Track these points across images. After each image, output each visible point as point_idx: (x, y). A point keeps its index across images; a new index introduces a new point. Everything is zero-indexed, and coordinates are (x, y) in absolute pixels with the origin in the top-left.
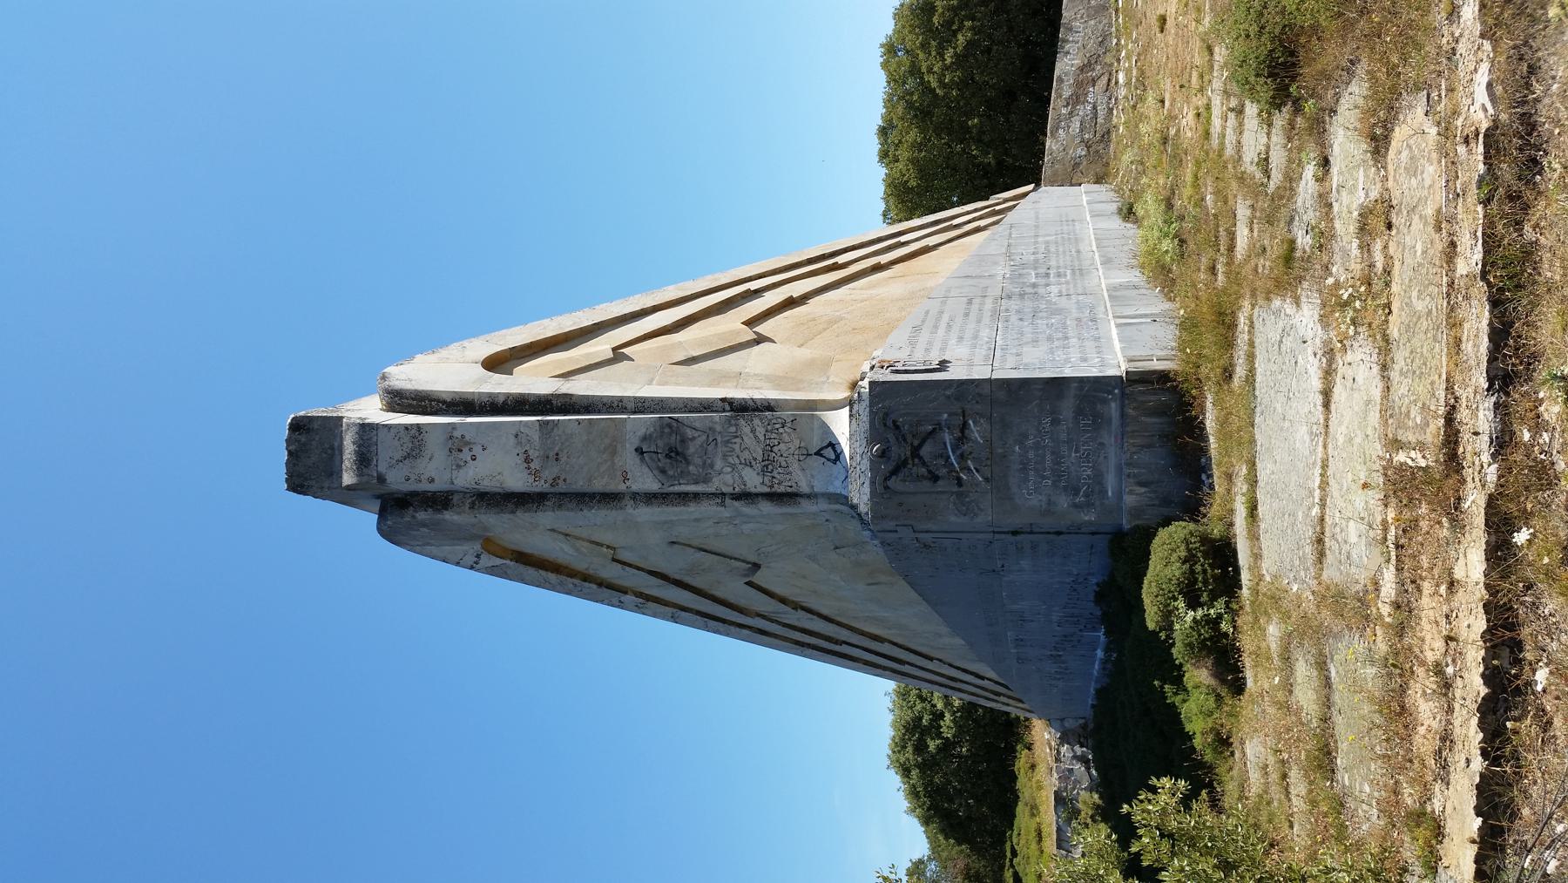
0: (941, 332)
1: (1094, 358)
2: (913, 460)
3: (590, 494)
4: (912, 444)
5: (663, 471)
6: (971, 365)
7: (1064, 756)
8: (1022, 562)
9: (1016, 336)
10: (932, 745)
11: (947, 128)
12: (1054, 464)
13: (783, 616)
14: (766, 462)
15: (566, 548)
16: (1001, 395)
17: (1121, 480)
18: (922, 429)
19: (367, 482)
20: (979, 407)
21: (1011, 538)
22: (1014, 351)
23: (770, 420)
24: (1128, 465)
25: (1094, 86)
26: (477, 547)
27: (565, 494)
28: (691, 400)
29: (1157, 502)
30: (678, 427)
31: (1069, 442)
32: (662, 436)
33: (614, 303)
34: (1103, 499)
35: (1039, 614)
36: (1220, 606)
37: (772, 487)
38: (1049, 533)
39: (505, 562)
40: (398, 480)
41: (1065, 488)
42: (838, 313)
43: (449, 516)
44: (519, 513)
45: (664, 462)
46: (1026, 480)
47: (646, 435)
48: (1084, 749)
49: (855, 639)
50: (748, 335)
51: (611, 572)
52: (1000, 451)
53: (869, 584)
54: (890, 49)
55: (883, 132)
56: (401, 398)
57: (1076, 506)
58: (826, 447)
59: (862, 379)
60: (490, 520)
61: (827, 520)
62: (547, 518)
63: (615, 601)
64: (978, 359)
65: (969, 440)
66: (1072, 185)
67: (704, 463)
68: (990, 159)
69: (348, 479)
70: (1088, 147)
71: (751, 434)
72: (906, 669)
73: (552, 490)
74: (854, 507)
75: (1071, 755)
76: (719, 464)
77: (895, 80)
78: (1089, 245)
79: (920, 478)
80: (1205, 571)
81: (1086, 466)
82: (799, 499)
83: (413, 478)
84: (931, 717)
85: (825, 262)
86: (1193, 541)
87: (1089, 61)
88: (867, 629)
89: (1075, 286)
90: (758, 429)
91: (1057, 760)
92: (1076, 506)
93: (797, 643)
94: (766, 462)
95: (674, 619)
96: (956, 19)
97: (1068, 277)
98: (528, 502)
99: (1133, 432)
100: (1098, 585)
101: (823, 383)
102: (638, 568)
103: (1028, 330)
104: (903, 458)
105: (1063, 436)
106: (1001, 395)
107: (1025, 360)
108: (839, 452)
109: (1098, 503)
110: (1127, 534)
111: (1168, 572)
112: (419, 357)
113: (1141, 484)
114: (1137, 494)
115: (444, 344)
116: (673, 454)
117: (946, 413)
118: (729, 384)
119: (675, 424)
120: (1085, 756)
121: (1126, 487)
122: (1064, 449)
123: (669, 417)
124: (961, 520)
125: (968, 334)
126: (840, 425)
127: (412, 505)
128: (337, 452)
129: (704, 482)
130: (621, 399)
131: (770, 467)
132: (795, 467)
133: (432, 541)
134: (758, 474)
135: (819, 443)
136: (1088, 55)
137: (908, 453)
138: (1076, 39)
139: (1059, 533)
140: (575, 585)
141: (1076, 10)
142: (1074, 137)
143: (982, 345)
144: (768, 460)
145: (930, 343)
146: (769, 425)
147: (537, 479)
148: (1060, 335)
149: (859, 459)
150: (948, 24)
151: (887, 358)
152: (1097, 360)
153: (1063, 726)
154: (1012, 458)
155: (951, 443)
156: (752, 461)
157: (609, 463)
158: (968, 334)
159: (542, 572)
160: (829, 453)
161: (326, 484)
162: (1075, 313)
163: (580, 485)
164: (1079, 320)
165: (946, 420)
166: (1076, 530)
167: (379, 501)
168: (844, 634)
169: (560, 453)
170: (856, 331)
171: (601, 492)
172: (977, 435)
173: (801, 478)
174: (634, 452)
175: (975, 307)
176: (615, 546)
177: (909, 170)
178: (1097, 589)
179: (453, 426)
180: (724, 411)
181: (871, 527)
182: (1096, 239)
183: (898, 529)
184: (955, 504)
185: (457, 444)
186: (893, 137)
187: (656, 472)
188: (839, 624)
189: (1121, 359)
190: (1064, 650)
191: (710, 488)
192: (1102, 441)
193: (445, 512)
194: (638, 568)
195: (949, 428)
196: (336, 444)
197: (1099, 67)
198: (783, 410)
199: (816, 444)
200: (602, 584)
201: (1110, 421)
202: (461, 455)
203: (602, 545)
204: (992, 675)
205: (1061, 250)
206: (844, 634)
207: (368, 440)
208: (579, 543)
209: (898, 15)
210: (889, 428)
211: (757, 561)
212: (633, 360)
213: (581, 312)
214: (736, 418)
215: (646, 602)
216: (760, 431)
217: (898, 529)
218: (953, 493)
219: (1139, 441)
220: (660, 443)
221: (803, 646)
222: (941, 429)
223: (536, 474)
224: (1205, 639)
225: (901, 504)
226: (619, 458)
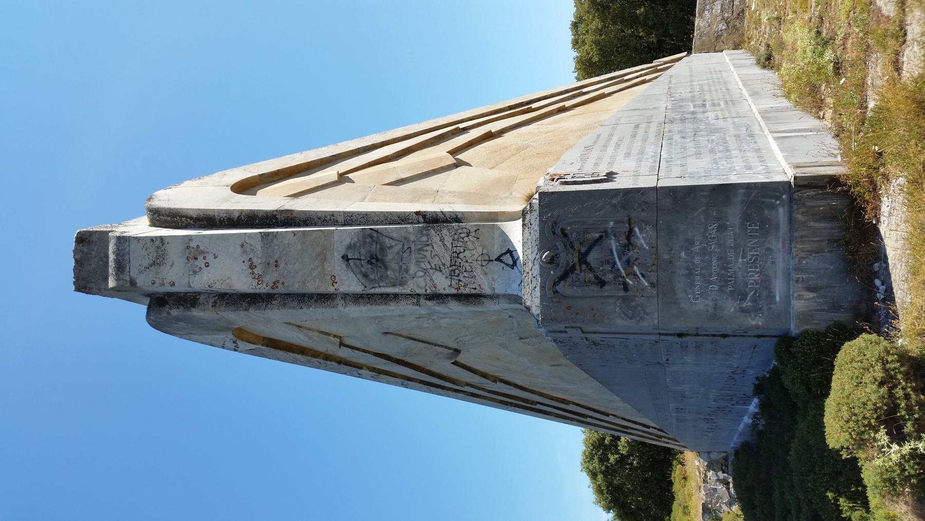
0: (610, 150)
2: (580, 266)
3: (309, 294)
4: (579, 252)
5: (365, 276)
6: (637, 175)
7: (710, 479)
8: (685, 358)
9: (679, 150)
10: (612, 458)
11: (621, 17)
12: (722, 269)
13: (486, 385)
14: (454, 268)
15: (301, 336)
17: (789, 285)
18: (589, 236)
19: (123, 286)
20: (645, 214)
21: (676, 339)
22: (679, 162)
23: (457, 230)
24: (798, 269)
28: (391, 213)
29: (825, 307)
30: (377, 237)
31: (736, 247)
32: (364, 245)
33: (353, 141)
34: (771, 304)
35: (698, 393)
37: (458, 289)
38: (714, 335)
39: (258, 346)
41: (732, 294)
43: (195, 312)
44: (251, 310)
45: (367, 268)
46: (692, 285)
47: (350, 244)
48: (726, 475)
50: (451, 160)
51: (345, 353)
52: (666, 257)
53: (552, 366)
55: (575, 25)
56: (159, 215)
57: (743, 311)
60: (230, 315)
61: (510, 317)
63: (355, 373)
65: (634, 246)
66: (715, 52)
67: (401, 268)
68: (653, 38)
69: (111, 283)
70: (727, 23)
72: (589, 420)
75: (715, 479)
76: (413, 269)
79: (587, 283)
81: (753, 272)
82: (486, 301)
83: (158, 281)
84: (611, 438)
85: (524, 107)
86: (889, 360)
90: (446, 238)
91: (705, 481)
92: (743, 311)
94: (454, 268)
95: (403, 385)
98: (259, 302)
99: (802, 237)
101: (506, 197)
103: (690, 145)
104: (571, 264)
105: (730, 242)
106: (667, 202)
108: (516, 258)
109: (765, 308)
110: (794, 339)
112: (186, 183)
113: (810, 289)
114: (805, 299)
116: (374, 261)
117: (612, 221)
118: (427, 200)
119: (375, 235)
120: (726, 480)
121: (793, 293)
122: (731, 255)
123: (371, 229)
125: (635, 150)
126: (515, 232)
127: (168, 304)
130: (332, 214)
131: (457, 272)
132: (478, 271)
134: (446, 277)
135: (499, 250)
137: (576, 260)
139: (724, 336)
143: (648, 159)
144: (455, 265)
145: (599, 159)
146: (455, 234)
147: (260, 283)
148: (721, 148)
149: (530, 264)
152: (761, 168)
153: (709, 457)
154: (678, 263)
155: (617, 250)
156: (441, 266)
157: (320, 269)
160: (508, 259)
162: (733, 132)
163: (296, 288)
164: (737, 136)
165: (612, 228)
166: (743, 334)
167: (149, 298)
168: (537, 398)
169: (279, 260)
170: (539, 155)
172: (643, 242)
173: (484, 283)
174: (341, 259)
175: (641, 131)
176: (341, 335)
177: (592, 49)
178: (757, 382)
179: (190, 238)
180: (419, 222)
182: (742, 81)
183: (567, 330)
186: (582, 27)
187: (360, 277)
191: (406, 290)
192: (769, 246)
193: (193, 310)
195: (615, 236)
198: (470, 221)
199: (496, 251)
200: (340, 361)
201: (777, 226)
202: (197, 263)
206: (537, 398)
207: (122, 250)
208: (311, 333)
210: (557, 235)
211: (458, 348)
212: (354, 182)
213: (326, 147)
214: (427, 229)
215: (378, 374)
216: (448, 240)
217: (567, 330)
218: (620, 297)
219: (807, 246)
220: (363, 251)
221: (507, 405)
222: (607, 236)
223: (259, 279)
226: (328, 264)
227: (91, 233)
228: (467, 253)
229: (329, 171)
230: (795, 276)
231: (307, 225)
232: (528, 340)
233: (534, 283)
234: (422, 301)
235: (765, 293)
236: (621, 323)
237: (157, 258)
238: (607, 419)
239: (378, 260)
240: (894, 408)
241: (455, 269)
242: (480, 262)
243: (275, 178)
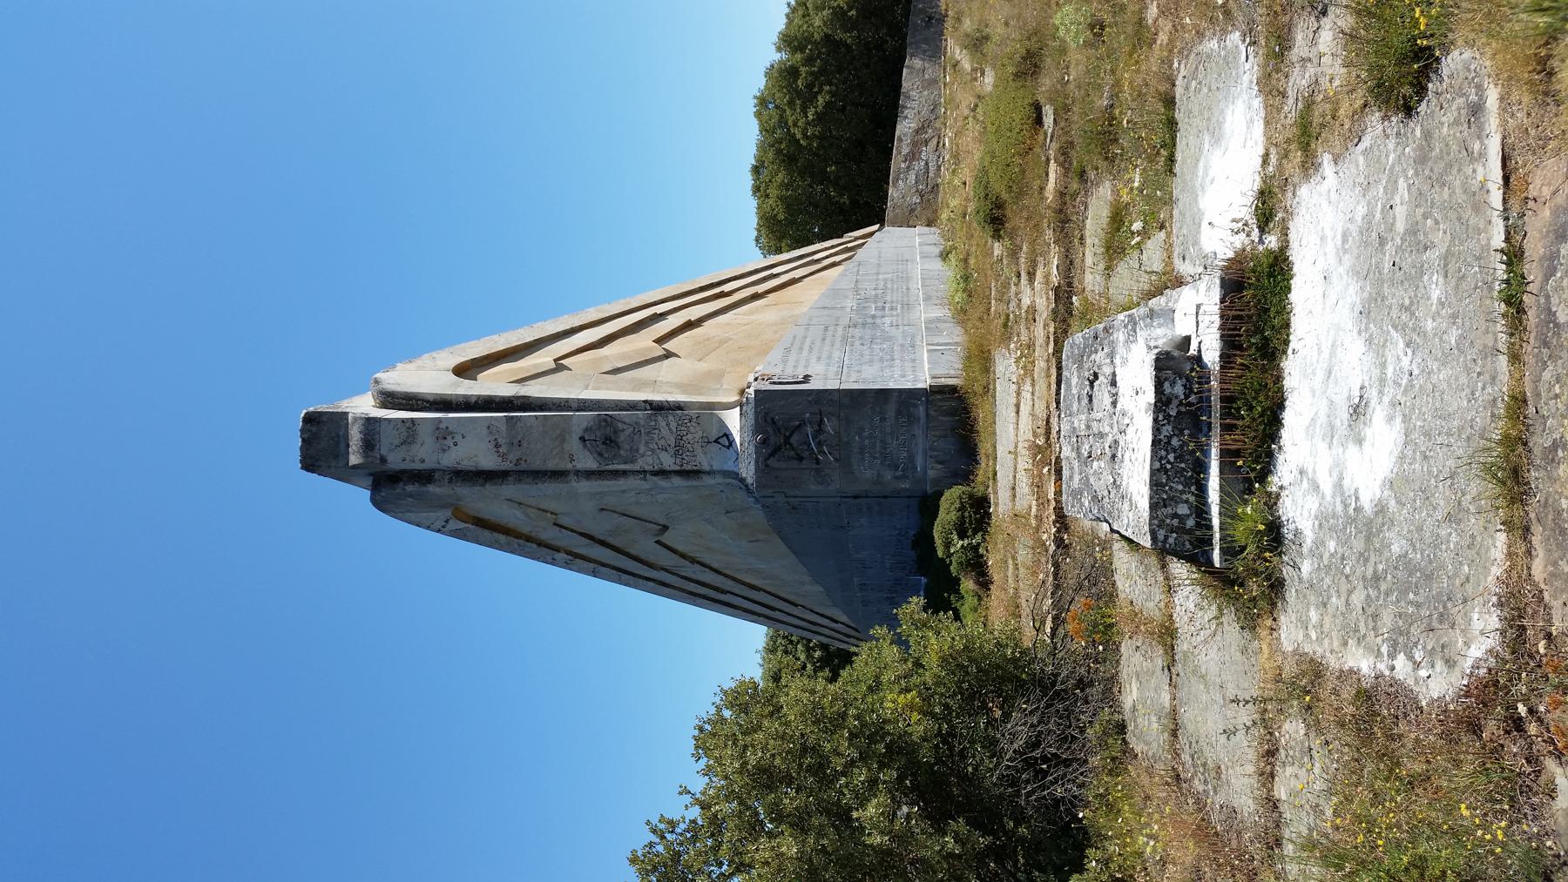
0: (805, 353)
1: (909, 375)
4: (785, 434)
5: (600, 454)
14: (678, 448)
15: (519, 514)
18: (792, 424)
21: (852, 501)
24: (931, 449)
25: (926, 146)
26: (448, 513)
27: (524, 471)
28: (621, 401)
30: (612, 422)
33: (547, 322)
35: (876, 562)
36: (978, 537)
37: (682, 466)
39: (467, 525)
40: (396, 461)
42: (726, 335)
43: (431, 488)
44: (488, 486)
46: (863, 459)
49: (737, 589)
50: (659, 351)
51: (550, 534)
52: (846, 440)
54: (762, 102)
55: (756, 170)
58: (722, 437)
59: (749, 387)
61: (721, 491)
62: (509, 490)
63: (549, 558)
64: (831, 375)
65: (824, 432)
66: (909, 226)
67: (631, 448)
68: (845, 199)
69: (354, 459)
70: (922, 197)
71: (666, 428)
72: (776, 615)
73: (514, 469)
74: (742, 480)
76: (642, 449)
77: (766, 130)
78: (917, 284)
79: (790, 458)
80: (970, 516)
82: (703, 476)
85: (713, 290)
87: (923, 125)
88: (748, 580)
89: (903, 319)
92: (896, 478)
93: (691, 593)
94: (678, 448)
95: (595, 574)
96: (817, 83)
97: (899, 311)
100: (914, 535)
102: (572, 531)
104: (778, 444)
105: (888, 430)
107: (863, 376)
109: (911, 476)
111: (948, 517)
115: (418, 355)
116: (608, 442)
118: (646, 390)
124: (820, 487)
126: (733, 421)
127: (401, 480)
128: (342, 439)
129: (632, 462)
130: (567, 400)
131: (681, 451)
132: (699, 451)
133: (413, 509)
136: (922, 120)
137: (782, 441)
138: (913, 106)
139: (885, 497)
140: (519, 545)
141: (913, 81)
142: (911, 187)
145: (797, 361)
150: (810, 86)
151: (767, 372)
159: (495, 534)
160: (724, 441)
161: (333, 464)
163: (537, 464)
164: (902, 345)
166: (897, 495)
167: (371, 478)
168: (729, 585)
171: (552, 469)
173: (703, 460)
174: (578, 441)
175: (830, 333)
177: (778, 206)
179: (439, 420)
180: (646, 410)
181: (755, 495)
184: (814, 476)
185: (443, 433)
187: (595, 455)
188: (726, 576)
189: (928, 376)
190: (896, 592)
191: (636, 467)
193: (429, 485)
194: (572, 531)
196: (341, 433)
197: (930, 131)
199: (714, 434)
200: (540, 544)
201: (919, 421)
203: (547, 512)
204: (844, 618)
205: (895, 286)
206: (729, 585)
208: (529, 510)
209: (769, 73)
215: (574, 560)
216: (673, 425)
217: (774, 495)
220: (598, 434)
222: (805, 424)
223: (503, 456)
224: (970, 559)
225: (776, 477)
228: (689, 436)
229: (535, 358)
230: (929, 454)
231: (542, 410)
232: (732, 514)
233: (749, 460)
234: (648, 476)
235: (910, 466)
236: (814, 488)
237: (407, 438)
238: (796, 611)
239: (611, 441)
240: (963, 523)
242: (700, 444)
243: (486, 362)
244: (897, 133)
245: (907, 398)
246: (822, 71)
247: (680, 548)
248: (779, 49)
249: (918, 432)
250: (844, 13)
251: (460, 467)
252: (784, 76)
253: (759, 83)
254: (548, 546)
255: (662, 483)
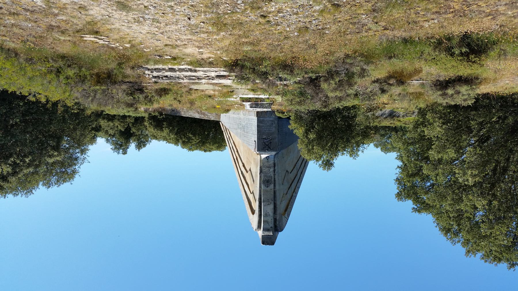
0: (250, 141)
5: (270, 183)
15: (284, 202)
16: (259, 133)
26: (283, 216)
40: (272, 225)
43: (278, 218)
50: (249, 172)
51: (289, 196)
54: (190, 149)
55: (205, 151)
62: (278, 203)
64: (254, 136)
69: (271, 234)
74: (276, 154)
79: (271, 145)
85: (236, 161)
115: (250, 223)
125: (250, 137)
126: (264, 156)
130: (259, 190)
132: (270, 163)
158: (250, 137)
160: (268, 158)
163: (272, 196)
166: (278, 123)
173: (272, 162)
185: (266, 215)
191: (273, 176)
199: (267, 160)
216: (264, 168)
223: (271, 203)
227: (262, 241)
236: (277, 140)
241: (269, 167)
244: (199, 118)
245: (259, 121)
246: (184, 135)
247: (292, 168)
248: (178, 145)
249: (266, 119)
250: (171, 130)
251: (273, 212)
252: (184, 144)
253: (185, 150)
254: (292, 197)
255: (276, 171)
